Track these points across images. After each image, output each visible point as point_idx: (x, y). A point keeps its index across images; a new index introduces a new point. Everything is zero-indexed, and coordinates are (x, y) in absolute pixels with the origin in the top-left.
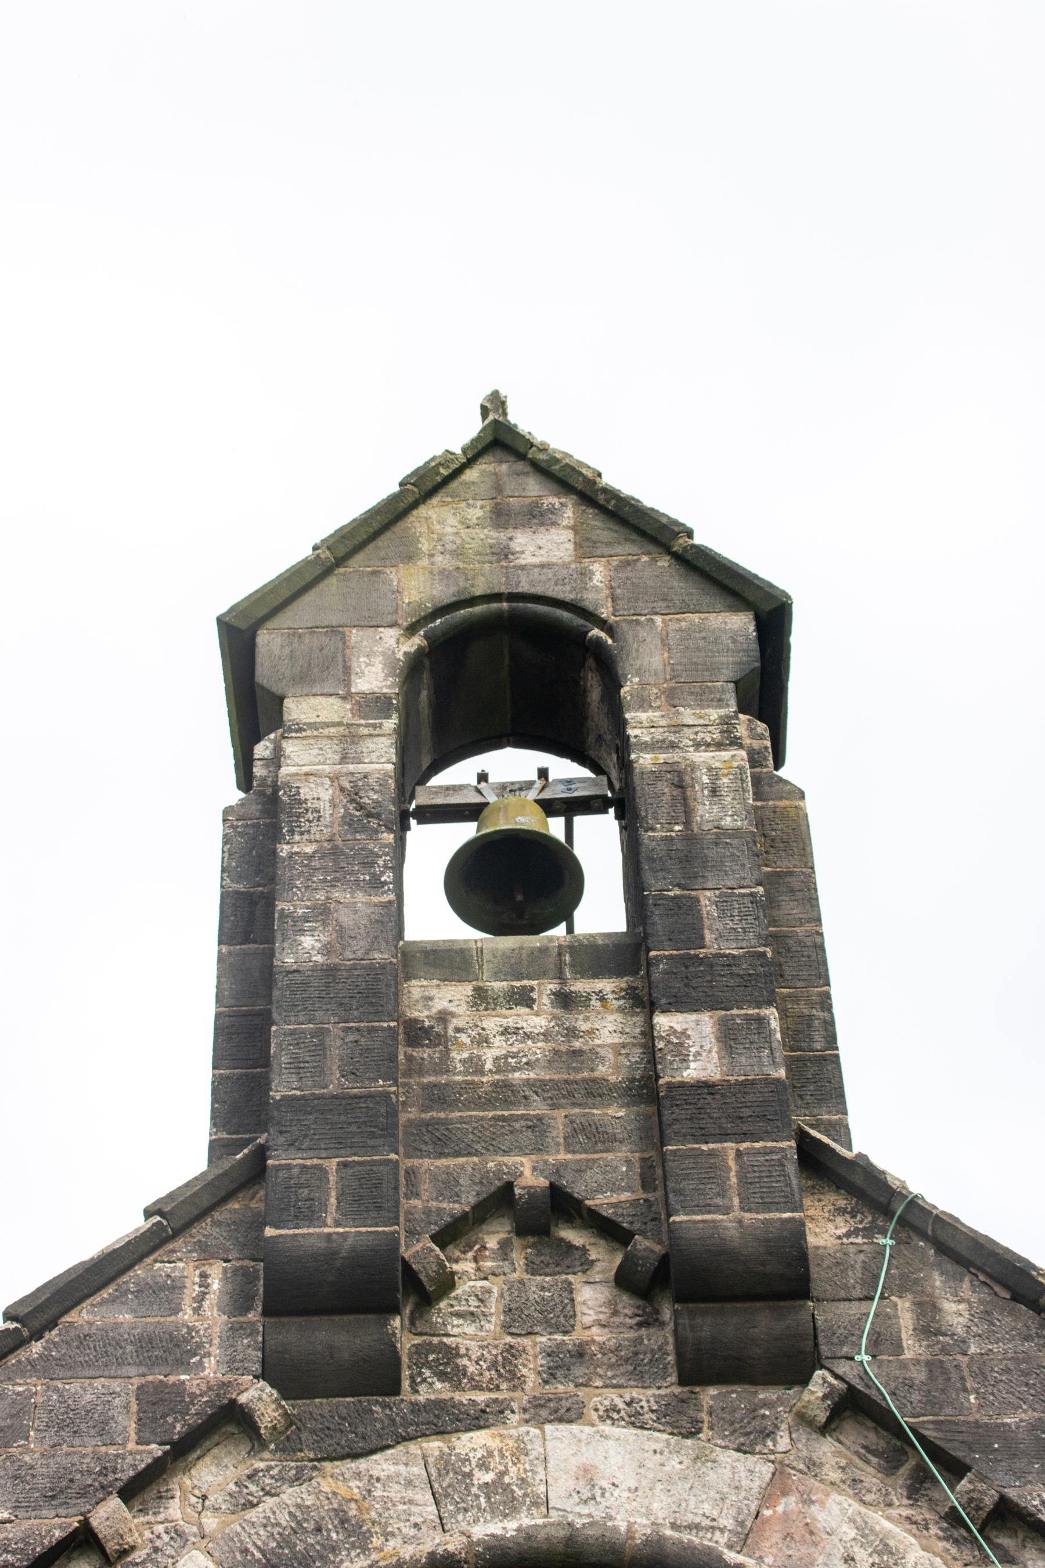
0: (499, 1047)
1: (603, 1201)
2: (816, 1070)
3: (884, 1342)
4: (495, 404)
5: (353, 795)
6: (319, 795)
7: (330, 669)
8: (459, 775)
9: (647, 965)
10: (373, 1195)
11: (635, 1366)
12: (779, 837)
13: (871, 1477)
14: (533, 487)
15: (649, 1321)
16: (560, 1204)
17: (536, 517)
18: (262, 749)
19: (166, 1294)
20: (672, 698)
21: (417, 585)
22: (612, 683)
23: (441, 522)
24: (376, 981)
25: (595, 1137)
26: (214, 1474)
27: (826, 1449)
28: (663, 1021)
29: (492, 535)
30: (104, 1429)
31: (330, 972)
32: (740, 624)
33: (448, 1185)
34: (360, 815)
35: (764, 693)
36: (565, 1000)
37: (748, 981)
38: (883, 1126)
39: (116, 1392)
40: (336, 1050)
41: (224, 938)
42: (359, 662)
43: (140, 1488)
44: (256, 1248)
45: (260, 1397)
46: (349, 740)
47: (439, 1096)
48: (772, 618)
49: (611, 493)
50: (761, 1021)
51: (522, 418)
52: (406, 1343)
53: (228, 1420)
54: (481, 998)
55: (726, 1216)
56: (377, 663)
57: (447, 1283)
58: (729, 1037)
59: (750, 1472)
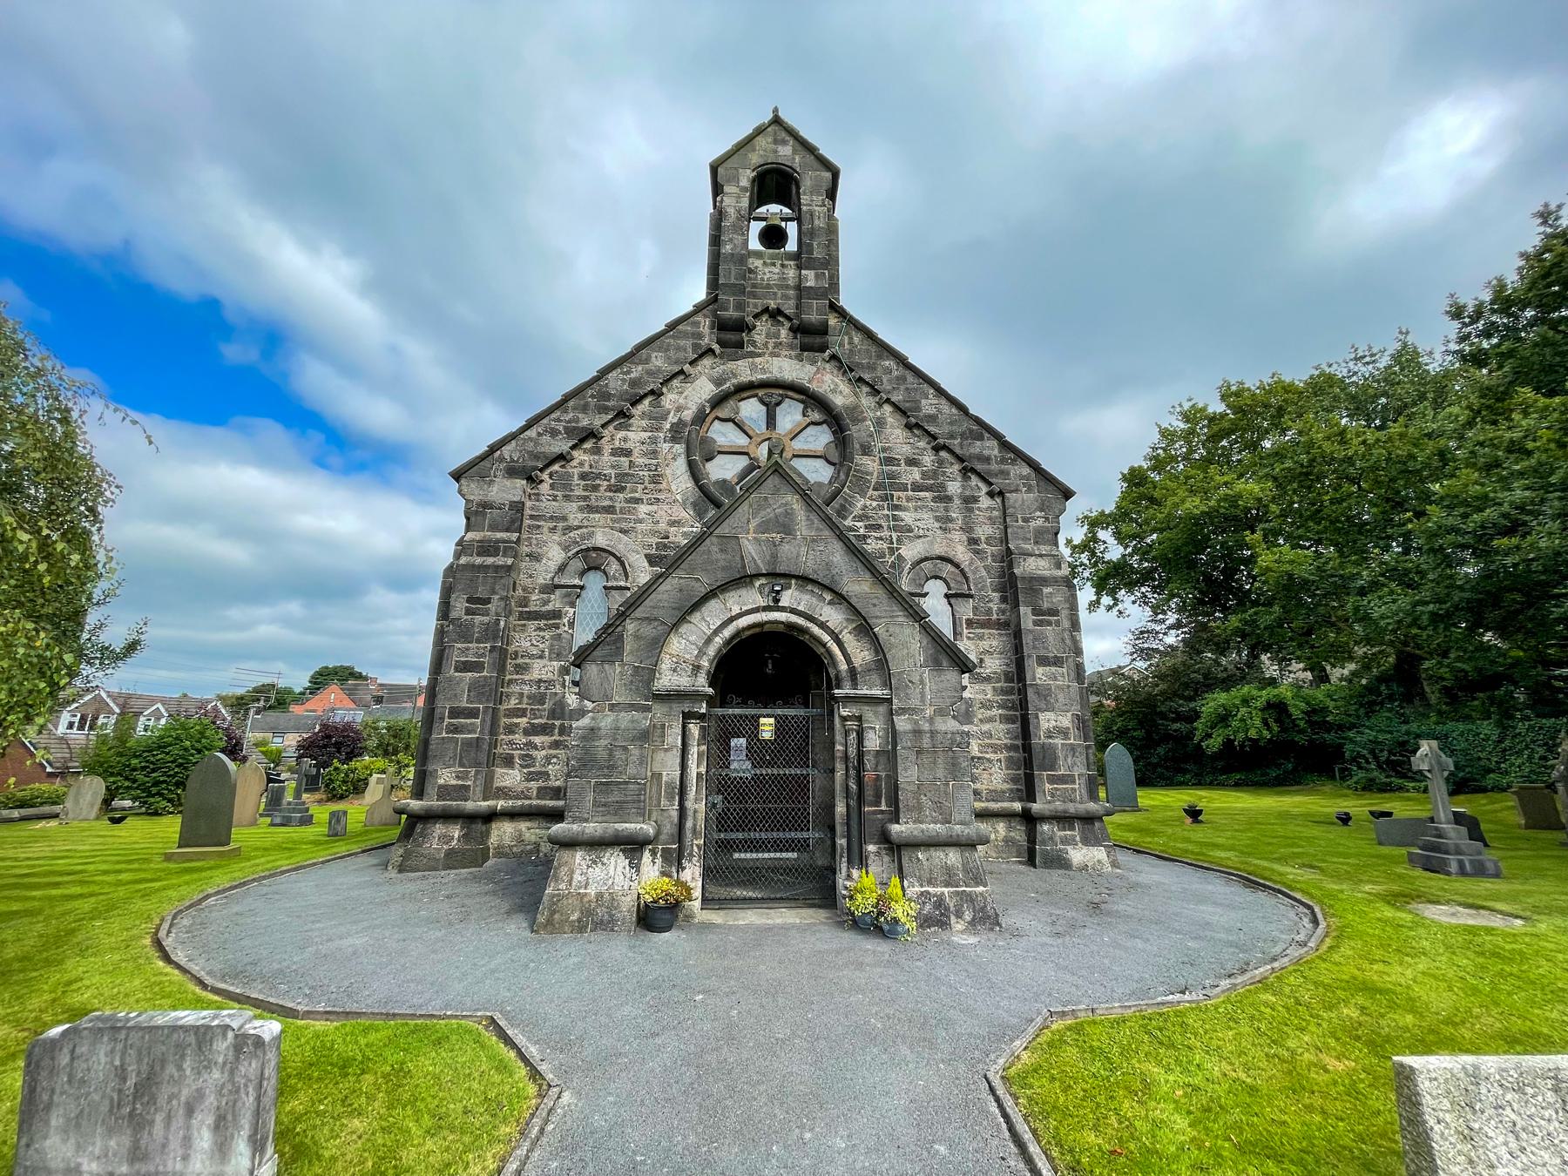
2: (834, 286)
3: (841, 345)
4: (776, 110)
8: (763, 209)
10: (740, 306)
11: (791, 347)
14: (783, 134)
16: (779, 312)
19: (697, 324)
21: (755, 159)
26: (707, 362)
36: (783, 266)
39: (688, 343)
45: (716, 347)
53: (710, 351)
56: (746, 177)
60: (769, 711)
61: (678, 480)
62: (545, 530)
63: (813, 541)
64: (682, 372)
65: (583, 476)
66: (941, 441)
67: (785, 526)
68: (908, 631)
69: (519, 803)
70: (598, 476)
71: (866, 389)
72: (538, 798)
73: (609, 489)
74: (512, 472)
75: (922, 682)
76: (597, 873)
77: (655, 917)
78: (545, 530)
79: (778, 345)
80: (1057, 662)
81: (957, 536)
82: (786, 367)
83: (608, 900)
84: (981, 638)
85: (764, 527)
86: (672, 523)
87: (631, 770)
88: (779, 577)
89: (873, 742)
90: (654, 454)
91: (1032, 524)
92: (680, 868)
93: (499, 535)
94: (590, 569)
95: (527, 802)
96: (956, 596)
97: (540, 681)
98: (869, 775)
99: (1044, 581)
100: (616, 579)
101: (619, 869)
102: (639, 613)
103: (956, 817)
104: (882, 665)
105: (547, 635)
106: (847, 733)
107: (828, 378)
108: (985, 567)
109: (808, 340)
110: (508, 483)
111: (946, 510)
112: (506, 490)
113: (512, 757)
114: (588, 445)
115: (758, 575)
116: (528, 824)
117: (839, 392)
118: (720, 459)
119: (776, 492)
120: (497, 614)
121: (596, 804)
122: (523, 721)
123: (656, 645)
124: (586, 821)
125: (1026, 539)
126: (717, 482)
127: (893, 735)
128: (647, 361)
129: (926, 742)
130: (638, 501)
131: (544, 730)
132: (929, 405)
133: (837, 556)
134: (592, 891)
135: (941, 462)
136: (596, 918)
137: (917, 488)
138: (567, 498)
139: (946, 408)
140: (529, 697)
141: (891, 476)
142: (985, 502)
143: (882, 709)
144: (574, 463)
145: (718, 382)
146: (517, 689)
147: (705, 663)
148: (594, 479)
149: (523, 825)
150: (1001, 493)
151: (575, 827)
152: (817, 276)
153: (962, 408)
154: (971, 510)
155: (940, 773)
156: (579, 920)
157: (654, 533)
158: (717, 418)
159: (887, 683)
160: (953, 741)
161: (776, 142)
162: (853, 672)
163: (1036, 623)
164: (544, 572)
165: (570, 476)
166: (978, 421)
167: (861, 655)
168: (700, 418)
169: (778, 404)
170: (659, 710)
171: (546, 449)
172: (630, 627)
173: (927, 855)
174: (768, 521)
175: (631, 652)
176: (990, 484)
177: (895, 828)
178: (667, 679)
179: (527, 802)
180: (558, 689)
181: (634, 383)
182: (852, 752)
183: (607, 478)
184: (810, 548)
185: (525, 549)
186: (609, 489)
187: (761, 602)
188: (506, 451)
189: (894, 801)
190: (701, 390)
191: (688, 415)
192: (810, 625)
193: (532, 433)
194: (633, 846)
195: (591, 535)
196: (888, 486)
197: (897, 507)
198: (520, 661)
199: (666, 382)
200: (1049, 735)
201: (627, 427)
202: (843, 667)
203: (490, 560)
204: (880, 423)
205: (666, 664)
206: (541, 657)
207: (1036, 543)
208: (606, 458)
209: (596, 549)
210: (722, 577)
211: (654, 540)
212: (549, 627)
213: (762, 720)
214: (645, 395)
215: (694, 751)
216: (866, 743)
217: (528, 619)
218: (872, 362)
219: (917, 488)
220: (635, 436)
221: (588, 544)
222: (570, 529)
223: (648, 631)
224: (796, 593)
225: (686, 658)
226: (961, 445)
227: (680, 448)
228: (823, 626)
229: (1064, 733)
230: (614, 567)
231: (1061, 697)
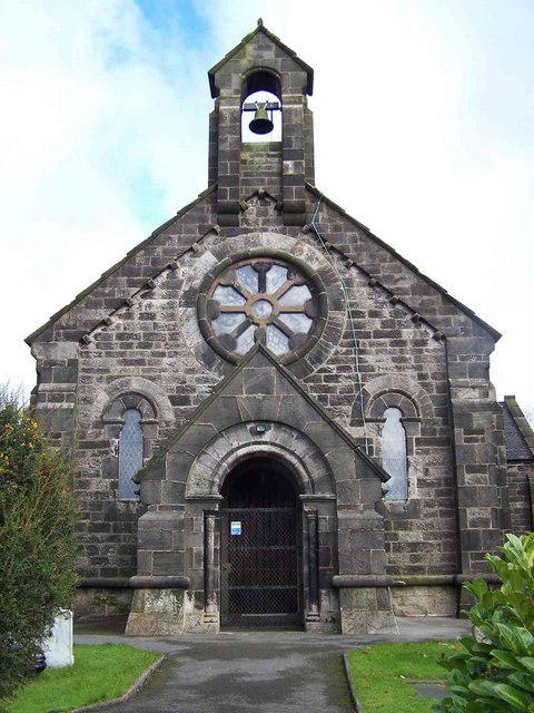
2: (311, 171)
3: (317, 220)
4: (260, 21)
7: (227, 84)
8: (251, 99)
9: (280, 150)
14: (267, 41)
21: (245, 63)
26: (211, 238)
38: (322, 183)
43: (199, 241)
48: (310, 73)
50: (301, 163)
51: (264, 25)
53: (214, 231)
56: (237, 79)
59: (293, 240)
61: (191, 337)
64: (191, 249)
65: (120, 337)
68: (348, 455)
71: (336, 256)
74: (68, 337)
80: (481, 469)
82: (273, 240)
84: (427, 452)
86: (189, 371)
89: (324, 527)
90: (172, 316)
92: (206, 604)
96: (409, 420)
99: (473, 407)
104: (330, 477)
107: (306, 247)
109: (287, 217)
111: (402, 352)
112: (66, 350)
114: (123, 311)
115: (249, 422)
117: (311, 255)
121: (155, 565)
123: (185, 469)
126: (220, 337)
127: (335, 522)
130: (163, 355)
131: (102, 528)
132: (385, 268)
133: (301, 407)
135: (396, 314)
137: (378, 335)
138: (108, 354)
141: (358, 326)
142: (432, 345)
144: (113, 327)
145: (219, 255)
151: (144, 577)
152: (295, 165)
154: (421, 351)
161: (260, 48)
163: (466, 440)
164: (95, 412)
167: (317, 472)
168: (207, 284)
169: (268, 270)
176: (435, 330)
178: (192, 490)
180: (111, 498)
182: (312, 534)
183: (137, 337)
184: (280, 400)
185: (81, 395)
186: (140, 346)
189: (336, 562)
190: (207, 260)
191: (197, 283)
192: (283, 453)
195: (128, 383)
196: (356, 334)
197: (362, 352)
198: (82, 478)
200: (474, 524)
202: (306, 479)
205: (192, 479)
206: (97, 476)
209: (132, 393)
211: (174, 385)
212: (101, 453)
215: (212, 535)
219: (378, 335)
220: (158, 302)
221: (126, 389)
222: (111, 378)
223: (180, 459)
225: (206, 474)
228: (292, 453)
229: (485, 522)
230: (146, 408)
231: (483, 496)
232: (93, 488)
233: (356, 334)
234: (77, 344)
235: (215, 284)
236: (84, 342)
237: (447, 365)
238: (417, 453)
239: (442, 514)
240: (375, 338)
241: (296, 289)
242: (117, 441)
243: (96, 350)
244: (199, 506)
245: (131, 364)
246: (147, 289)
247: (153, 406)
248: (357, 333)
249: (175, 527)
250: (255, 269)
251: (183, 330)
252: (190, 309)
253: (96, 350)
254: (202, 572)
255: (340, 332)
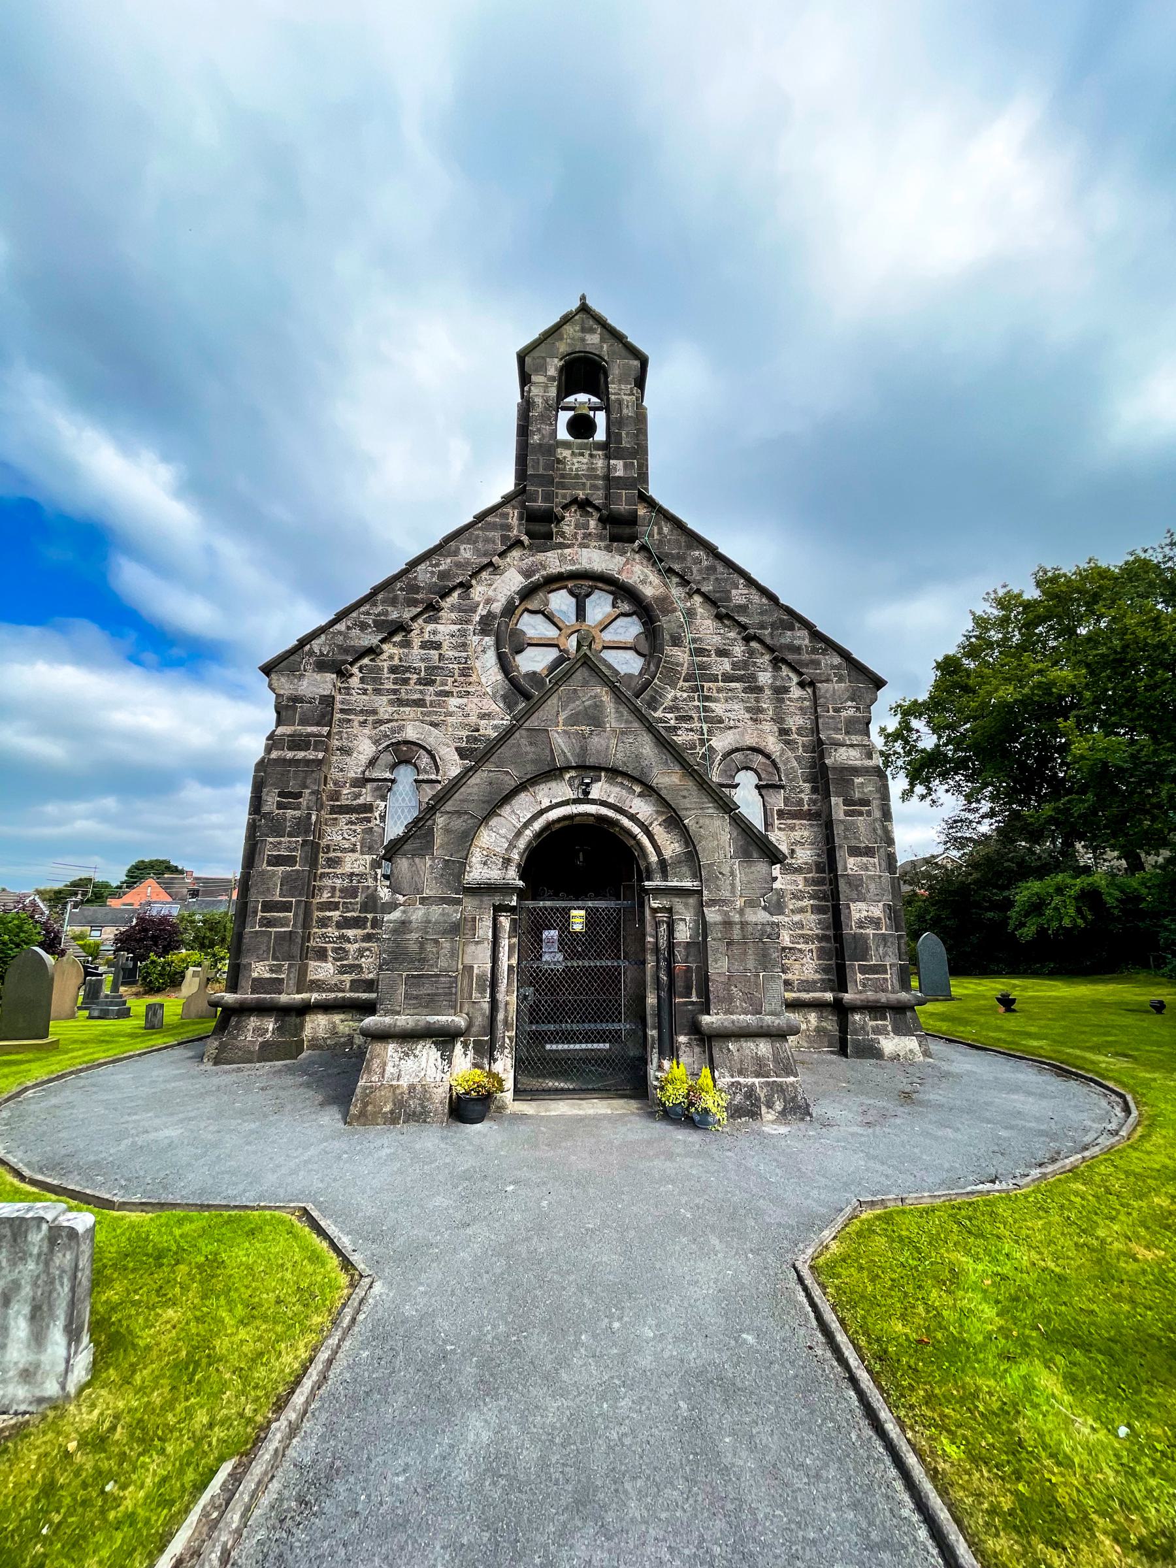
0: (577, 465)
1: (596, 502)
2: (643, 477)
3: (651, 535)
4: (583, 298)
5: (547, 401)
6: (539, 400)
7: (541, 368)
8: (571, 399)
9: (609, 449)
10: (548, 497)
11: (601, 538)
12: (640, 418)
13: (645, 562)
14: (591, 322)
15: (605, 528)
17: (592, 331)
18: (526, 388)
19: (506, 516)
20: (620, 382)
21: (563, 348)
22: (606, 377)
23: (570, 330)
24: (551, 447)
25: (594, 487)
26: (516, 553)
27: (637, 556)
28: (612, 462)
29: (580, 334)
30: (494, 542)
31: (540, 445)
32: (636, 363)
33: (564, 496)
34: (548, 407)
35: (640, 382)
36: (591, 456)
37: (631, 453)
39: (496, 535)
40: (541, 463)
41: (518, 435)
42: (549, 367)
43: (502, 555)
44: (524, 507)
45: (525, 538)
46: (546, 387)
47: (563, 476)
48: (644, 362)
49: (610, 325)
51: (590, 302)
52: (555, 530)
53: (518, 543)
54: (573, 454)
55: (622, 507)
56: (553, 367)
57: (563, 518)
58: (625, 466)
60: (580, 903)
62: (356, 723)
63: (623, 733)
64: (490, 564)
65: (393, 670)
66: (751, 631)
67: (594, 718)
68: (718, 823)
69: (333, 995)
70: (408, 669)
71: (675, 580)
72: (351, 991)
73: (419, 682)
74: (322, 666)
75: (732, 873)
76: (409, 1065)
77: (467, 1108)
78: (356, 723)
79: (587, 536)
80: (869, 852)
81: (768, 726)
82: (595, 559)
83: (419, 1092)
85: (573, 720)
86: (483, 716)
87: (443, 963)
88: (588, 770)
89: (683, 933)
91: (844, 714)
93: (310, 729)
94: (400, 762)
95: (340, 995)
97: (352, 874)
98: (680, 966)
99: (856, 771)
100: (427, 773)
101: (432, 1061)
102: (449, 806)
103: (766, 1007)
104: (692, 857)
105: (359, 828)
106: (657, 925)
108: (797, 758)
109: (617, 530)
110: (318, 677)
111: (757, 700)
112: (315, 684)
113: (325, 950)
114: (397, 638)
115: (568, 768)
116: (342, 1016)
118: (530, 652)
119: (585, 684)
120: (309, 808)
122: (335, 914)
123: (467, 838)
124: (398, 1013)
125: (837, 730)
126: (527, 675)
127: (703, 926)
128: (456, 553)
129: (736, 933)
130: (448, 694)
131: (357, 923)
132: (739, 595)
133: (647, 748)
134: (404, 1083)
135: (751, 653)
136: (408, 1110)
137: (728, 678)
138: (377, 692)
139: (756, 598)
140: (341, 891)
141: (702, 666)
142: (796, 692)
143: (692, 901)
144: (384, 656)
145: (527, 574)
146: (328, 882)
147: (515, 856)
148: (404, 672)
149: (337, 1018)
150: (812, 684)
153: (772, 598)
154: (782, 701)
155: (751, 964)
156: (392, 1112)
157: (465, 726)
158: (527, 610)
159: (697, 874)
160: (763, 932)
161: (583, 330)
162: (662, 863)
163: (847, 813)
164: (355, 765)
165: (380, 669)
166: (789, 611)
167: (671, 847)
168: (510, 610)
169: (588, 595)
170: (469, 903)
171: (355, 643)
172: (440, 820)
173: (737, 1045)
174: (577, 714)
175: (442, 846)
176: (800, 674)
177: (706, 1019)
178: (477, 873)
179: (340, 995)
180: (370, 882)
181: (443, 575)
182: (663, 943)
183: (417, 671)
184: (620, 740)
185: (336, 743)
186: (419, 682)
187: (571, 794)
188: (316, 645)
189: (704, 992)
190: (510, 582)
191: (497, 607)
193: (341, 627)
194: (445, 1038)
195: (401, 729)
196: (699, 677)
198: (332, 855)
199: (474, 575)
201: (435, 620)
202: (654, 858)
203: (301, 755)
204: (690, 613)
205: (476, 858)
206: (353, 851)
207: (847, 733)
208: (416, 651)
209: (406, 742)
210: (531, 770)
213: (574, 913)
214: (454, 589)
215: (505, 943)
216: (677, 935)
217: (341, 813)
218: (684, 551)
219: (728, 678)
220: (445, 629)
221: (399, 737)
222: (381, 722)
223: (458, 824)
224: (606, 786)
225: (496, 850)
226: (771, 634)
227: (489, 641)
228: (633, 818)
229: (876, 923)
231: (872, 886)
232: (347, 869)
233: (699, 677)
234: (334, 676)
235: (521, 608)
236: (343, 675)
237: (817, 718)
238: (780, 829)
239: (816, 910)
240: (723, 681)
241: (621, 621)
242: (383, 804)
243: (360, 686)
244: (485, 899)
245: (407, 705)
246: (432, 610)
247: (433, 757)
248: (702, 675)
249: (444, 933)
250: (571, 593)
251: (478, 664)
252: (487, 639)
253: (360, 686)
254: (486, 1006)
255: (680, 673)
